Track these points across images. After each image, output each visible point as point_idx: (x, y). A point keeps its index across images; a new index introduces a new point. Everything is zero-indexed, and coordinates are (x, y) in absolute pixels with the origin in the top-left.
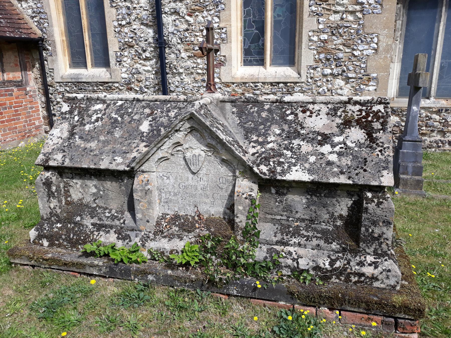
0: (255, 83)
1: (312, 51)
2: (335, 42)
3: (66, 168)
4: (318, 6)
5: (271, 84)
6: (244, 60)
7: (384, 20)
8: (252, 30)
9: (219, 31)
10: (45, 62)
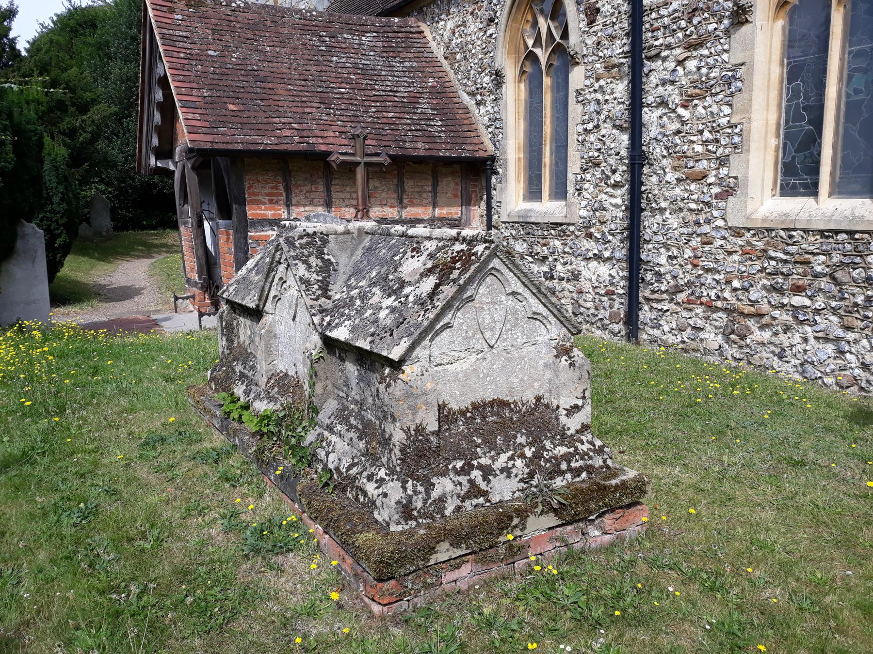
0: (789, 230)
5: (821, 232)
8: (801, 126)
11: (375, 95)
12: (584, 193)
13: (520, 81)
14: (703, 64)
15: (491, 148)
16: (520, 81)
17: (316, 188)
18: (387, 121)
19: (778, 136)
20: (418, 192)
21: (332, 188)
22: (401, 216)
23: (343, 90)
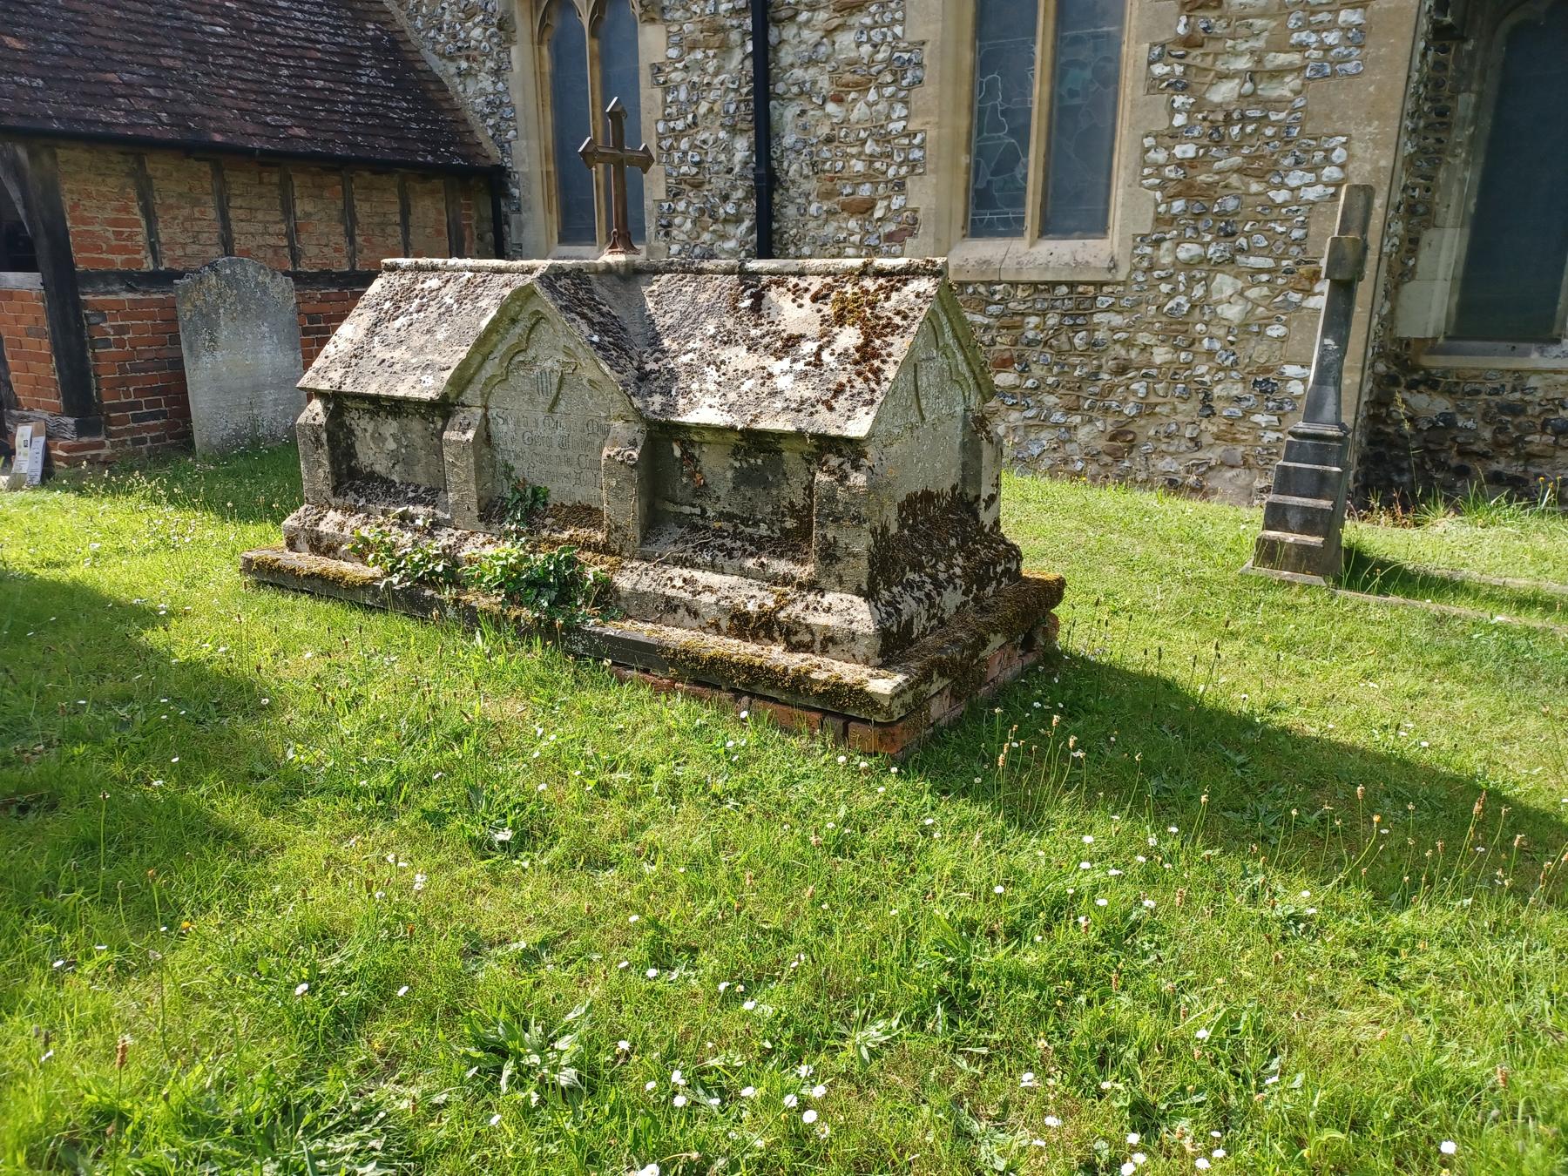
1: (1151, 193)
2: (1217, 165)
5: (1034, 285)
9: (906, 141)
11: (280, 45)
12: (675, 232)
13: (540, 42)
14: (864, 38)
15: (495, 153)
16: (540, 42)
17: (202, 213)
19: (969, 151)
21: (231, 214)
22: (353, 266)
23: (220, 29)
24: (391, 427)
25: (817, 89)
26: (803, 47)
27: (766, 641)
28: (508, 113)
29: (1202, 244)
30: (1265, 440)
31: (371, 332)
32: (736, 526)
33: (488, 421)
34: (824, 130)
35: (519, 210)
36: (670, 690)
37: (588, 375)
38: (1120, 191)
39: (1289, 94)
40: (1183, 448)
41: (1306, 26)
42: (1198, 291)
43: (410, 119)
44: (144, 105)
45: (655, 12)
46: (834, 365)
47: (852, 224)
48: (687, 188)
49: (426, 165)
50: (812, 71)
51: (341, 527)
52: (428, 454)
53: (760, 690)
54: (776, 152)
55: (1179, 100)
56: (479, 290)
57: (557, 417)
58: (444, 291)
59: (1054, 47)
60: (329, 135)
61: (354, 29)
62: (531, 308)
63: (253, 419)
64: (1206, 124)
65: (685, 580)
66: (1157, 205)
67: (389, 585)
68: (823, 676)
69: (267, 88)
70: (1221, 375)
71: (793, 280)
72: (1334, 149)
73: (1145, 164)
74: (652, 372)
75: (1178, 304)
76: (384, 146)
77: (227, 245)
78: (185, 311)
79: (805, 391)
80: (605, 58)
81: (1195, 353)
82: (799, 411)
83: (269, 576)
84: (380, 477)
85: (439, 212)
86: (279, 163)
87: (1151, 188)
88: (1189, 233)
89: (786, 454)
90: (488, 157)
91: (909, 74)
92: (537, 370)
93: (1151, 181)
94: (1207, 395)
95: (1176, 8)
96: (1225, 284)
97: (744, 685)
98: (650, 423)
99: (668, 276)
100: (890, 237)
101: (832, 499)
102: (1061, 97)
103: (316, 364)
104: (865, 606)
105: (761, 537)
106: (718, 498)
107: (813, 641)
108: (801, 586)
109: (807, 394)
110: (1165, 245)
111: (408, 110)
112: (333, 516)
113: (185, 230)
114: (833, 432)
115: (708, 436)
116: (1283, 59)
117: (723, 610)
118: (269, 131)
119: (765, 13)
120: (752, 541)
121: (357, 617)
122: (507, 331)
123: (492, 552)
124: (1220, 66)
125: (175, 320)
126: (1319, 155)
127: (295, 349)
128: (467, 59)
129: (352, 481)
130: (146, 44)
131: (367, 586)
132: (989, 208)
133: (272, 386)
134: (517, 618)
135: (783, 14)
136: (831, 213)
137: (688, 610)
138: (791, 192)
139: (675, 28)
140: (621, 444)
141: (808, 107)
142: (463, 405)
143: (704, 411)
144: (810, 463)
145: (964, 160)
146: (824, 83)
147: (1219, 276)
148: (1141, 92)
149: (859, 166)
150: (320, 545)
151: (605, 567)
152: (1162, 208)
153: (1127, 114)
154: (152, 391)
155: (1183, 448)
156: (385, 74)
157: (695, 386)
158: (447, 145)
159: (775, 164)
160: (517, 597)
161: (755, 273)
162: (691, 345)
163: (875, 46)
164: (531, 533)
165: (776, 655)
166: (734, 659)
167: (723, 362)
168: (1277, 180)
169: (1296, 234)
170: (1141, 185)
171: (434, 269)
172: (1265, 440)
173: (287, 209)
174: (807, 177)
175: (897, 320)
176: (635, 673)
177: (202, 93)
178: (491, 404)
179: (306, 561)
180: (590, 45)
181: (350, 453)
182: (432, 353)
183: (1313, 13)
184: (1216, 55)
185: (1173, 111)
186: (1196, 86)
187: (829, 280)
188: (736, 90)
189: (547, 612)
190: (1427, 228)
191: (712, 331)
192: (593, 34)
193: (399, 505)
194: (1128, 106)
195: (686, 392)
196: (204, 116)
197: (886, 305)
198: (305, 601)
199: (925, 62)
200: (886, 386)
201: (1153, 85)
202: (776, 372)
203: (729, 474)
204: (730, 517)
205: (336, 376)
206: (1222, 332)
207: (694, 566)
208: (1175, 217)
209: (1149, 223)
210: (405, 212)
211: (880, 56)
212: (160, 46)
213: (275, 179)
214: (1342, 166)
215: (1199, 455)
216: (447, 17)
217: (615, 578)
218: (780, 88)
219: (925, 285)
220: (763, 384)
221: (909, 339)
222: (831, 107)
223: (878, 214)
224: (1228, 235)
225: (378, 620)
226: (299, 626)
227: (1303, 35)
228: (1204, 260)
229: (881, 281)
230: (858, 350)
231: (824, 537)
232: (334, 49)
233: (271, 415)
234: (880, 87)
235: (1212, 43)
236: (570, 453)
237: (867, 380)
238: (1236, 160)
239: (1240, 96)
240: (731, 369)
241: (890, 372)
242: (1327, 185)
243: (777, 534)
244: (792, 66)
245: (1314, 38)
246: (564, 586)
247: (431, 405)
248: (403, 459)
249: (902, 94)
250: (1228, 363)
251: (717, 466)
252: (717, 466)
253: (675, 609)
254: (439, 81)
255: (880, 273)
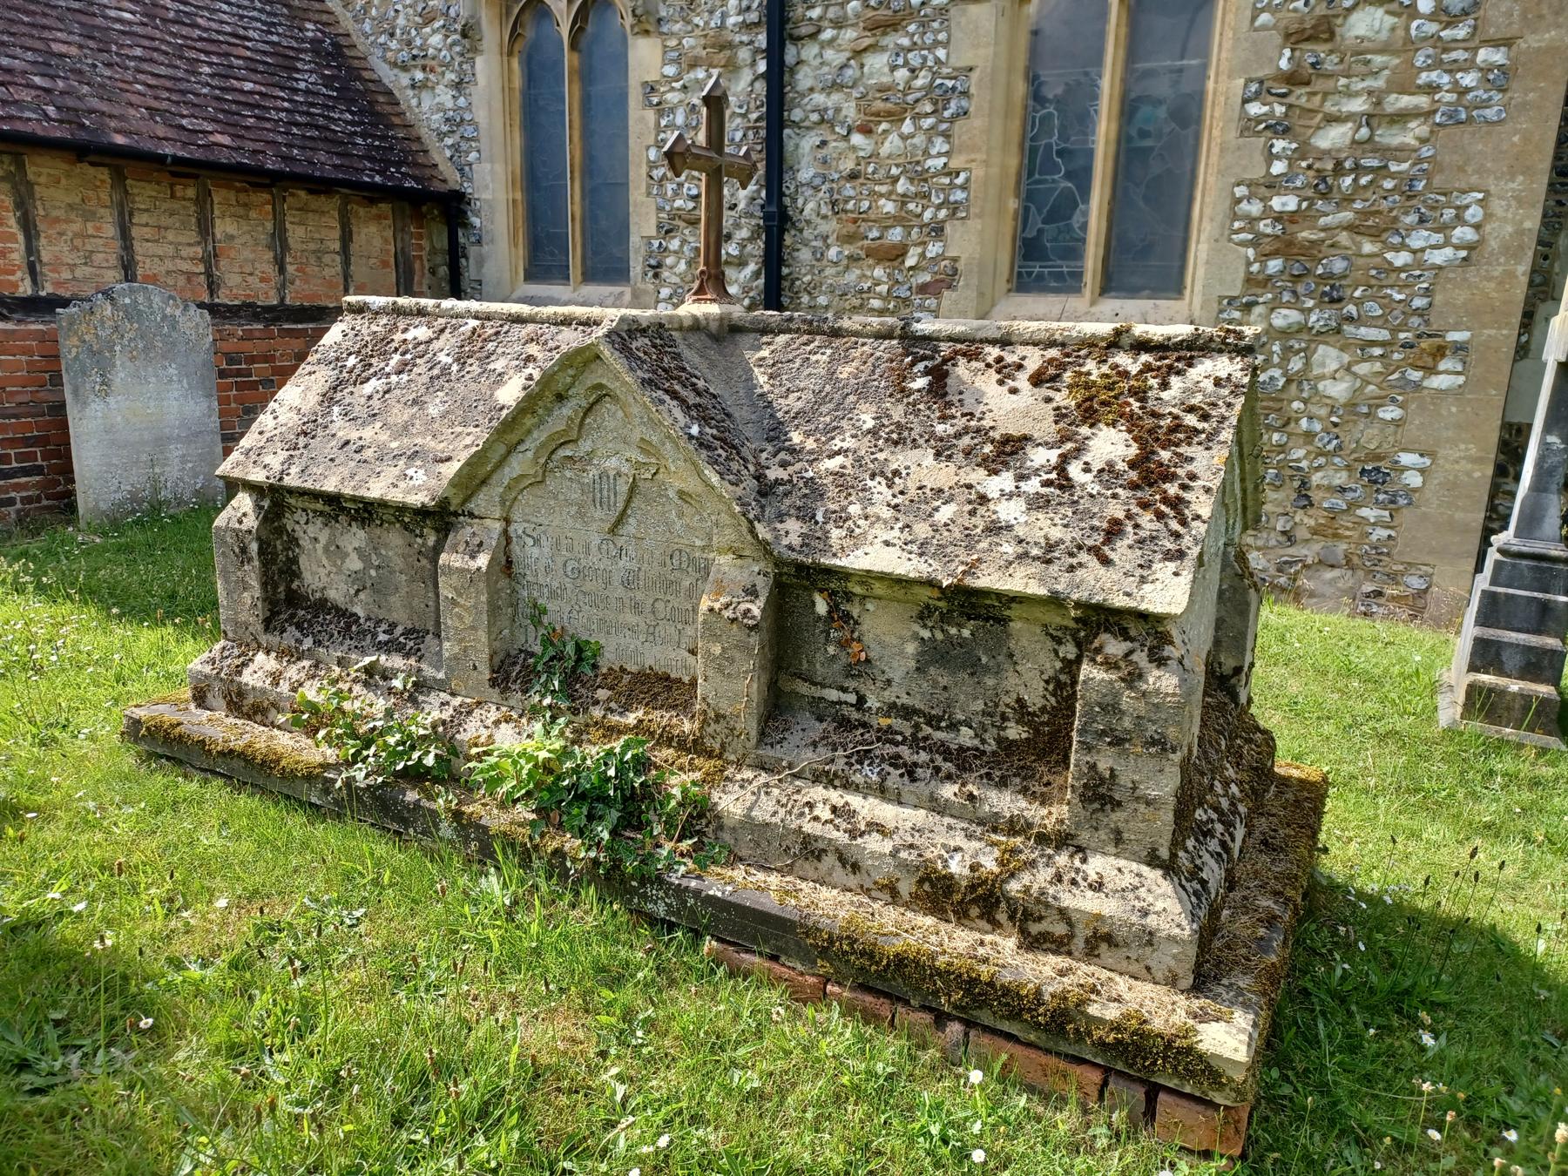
1: (1242, 250)
2: (1322, 221)
3: (291, 491)
4: (1272, 99)
6: (1020, 274)
7: (1514, 145)
8: (1054, 181)
9: (947, 181)
10: (463, 261)
11: (201, 39)
12: (665, 274)
13: (510, 54)
14: (900, 61)
15: (453, 179)
16: (510, 54)
17: (98, 229)
18: (242, 99)
19: (1017, 196)
20: (314, 252)
21: (135, 232)
22: (282, 299)
23: (127, 16)
24: (355, 538)
25: (841, 118)
26: (826, 69)
27: (983, 924)
28: (469, 131)
29: (1302, 311)
30: (1374, 538)
31: (328, 399)
32: (917, 727)
33: (508, 540)
34: (848, 165)
35: (479, 242)
36: (820, 997)
37: (678, 485)
38: (1203, 247)
39: (1413, 142)
40: (1273, 542)
41: (1438, 64)
42: (1296, 364)
43: (355, 133)
44: (26, 96)
45: (648, 22)
46: (1095, 488)
47: (879, 272)
48: (682, 224)
49: (372, 187)
50: (836, 97)
51: (276, 678)
52: (412, 580)
53: (985, 1017)
54: (789, 187)
55: (1279, 145)
56: (490, 346)
57: (621, 542)
58: (436, 345)
59: (1124, 81)
60: (259, 146)
61: (291, 27)
62: (591, 379)
63: (154, 480)
64: (1311, 173)
65: (834, 809)
66: (1249, 264)
67: (349, 782)
68: (1112, 1013)
69: (184, 86)
70: (1322, 460)
71: (993, 352)
72: (1467, 207)
73: (1235, 217)
74: (778, 482)
75: (1272, 378)
76: (324, 162)
77: (128, 269)
78: (70, 349)
79: (1048, 527)
80: (586, 76)
81: (1290, 435)
82: (1049, 562)
83: (164, 747)
84: (337, 608)
85: (386, 241)
86: (195, 174)
87: (1243, 244)
88: (1286, 297)
89: (1015, 626)
90: (444, 181)
91: (953, 104)
92: (593, 472)
93: (1243, 236)
94: (1304, 483)
95: (1279, 40)
96: (1328, 357)
97: (956, 1007)
98: (779, 563)
99: (782, 339)
100: (923, 289)
101: (1111, 707)
102: (1129, 139)
103: (245, 442)
104: (1166, 887)
105: (962, 749)
106: (889, 682)
107: (1071, 936)
108: (1042, 839)
109: (1056, 533)
110: (1258, 310)
111: (352, 123)
112: (264, 662)
113: (75, 248)
114: (1119, 601)
115: (879, 588)
116: (1406, 101)
117: (904, 865)
118: (184, 136)
119: (782, 29)
120: (947, 753)
121: (296, 822)
122: (549, 411)
123: (512, 740)
124: (1329, 107)
125: (57, 357)
126: (1449, 214)
127: (209, 396)
128: (424, 69)
129: (290, 609)
130: (33, 25)
131: (314, 776)
132: (1039, 260)
133: (178, 439)
134: (558, 853)
135: (804, 31)
136: (853, 259)
137: (842, 860)
138: (806, 233)
139: (673, 43)
140: (732, 588)
141: (829, 137)
142: (471, 515)
143: (876, 552)
144: (1059, 641)
145: (1013, 204)
146: (850, 112)
147: (1321, 348)
148: (1233, 134)
149: (889, 207)
150: (243, 704)
151: (697, 775)
152: (1255, 268)
153: (1214, 159)
154: (26, 442)
155: (1273, 542)
156: (328, 82)
157: (855, 509)
158: (399, 164)
159: (787, 201)
160: (555, 815)
161: (927, 339)
162: (837, 444)
163: (913, 71)
164: (575, 712)
165: (1003, 955)
166: (941, 961)
167: (896, 473)
168: (1396, 240)
169: (1419, 302)
170: (1230, 240)
171: (421, 312)
172: (1374, 538)
173: (205, 228)
174: (825, 217)
175: (1191, 420)
176: (757, 959)
177: (102, 86)
178: (516, 516)
179: (217, 726)
180: (569, 59)
181: (292, 570)
182: (422, 434)
183: (1446, 50)
184: (1326, 95)
185: (1271, 157)
186: (1298, 129)
187: (1053, 353)
188: (744, 116)
189: (609, 848)
190: (1543, 301)
191: (870, 424)
192: (574, 45)
193: (364, 653)
194: (1215, 150)
195: (842, 518)
196: (103, 113)
197: (1165, 395)
198: (216, 790)
199: (973, 90)
200: (1199, 528)
201: (1248, 126)
202: (993, 493)
203: (911, 648)
204: (907, 712)
205: (275, 461)
206: (1323, 412)
207: (848, 786)
208: (1270, 277)
209: (1239, 283)
210: (346, 238)
211: (919, 83)
212: (50, 29)
213: (191, 192)
214: (1477, 227)
215: (1291, 551)
216: (401, 21)
217: (715, 796)
218: (797, 115)
219: (1224, 366)
220: (972, 513)
221: (1219, 454)
222: (857, 139)
223: (910, 261)
224: (1333, 301)
225: (326, 835)
226: (209, 840)
227: (1434, 75)
228: (1303, 328)
229: (1145, 358)
230: (1133, 465)
231: (1093, 767)
232: (267, 48)
233: (176, 474)
234: (917, 117)
235: (1321, 81)
236: (639, 596)
237: (1160, 516)
238: (1347, 216)
239: (1354, 142)
240: (912, 485)
241: (1202, 505)
242: (1457, 248)
243: (991, 746)
244: (811, 90)
245: (1446, 79)
246: (632, 804)
247: (422, 513)
248: (372, 584)
249: (944, 126)
250: (1330, 447)
251: (892, 639)
252: (892, 639)
253: (818, 855)
254: (390, 93)
255: (1142, 346)
